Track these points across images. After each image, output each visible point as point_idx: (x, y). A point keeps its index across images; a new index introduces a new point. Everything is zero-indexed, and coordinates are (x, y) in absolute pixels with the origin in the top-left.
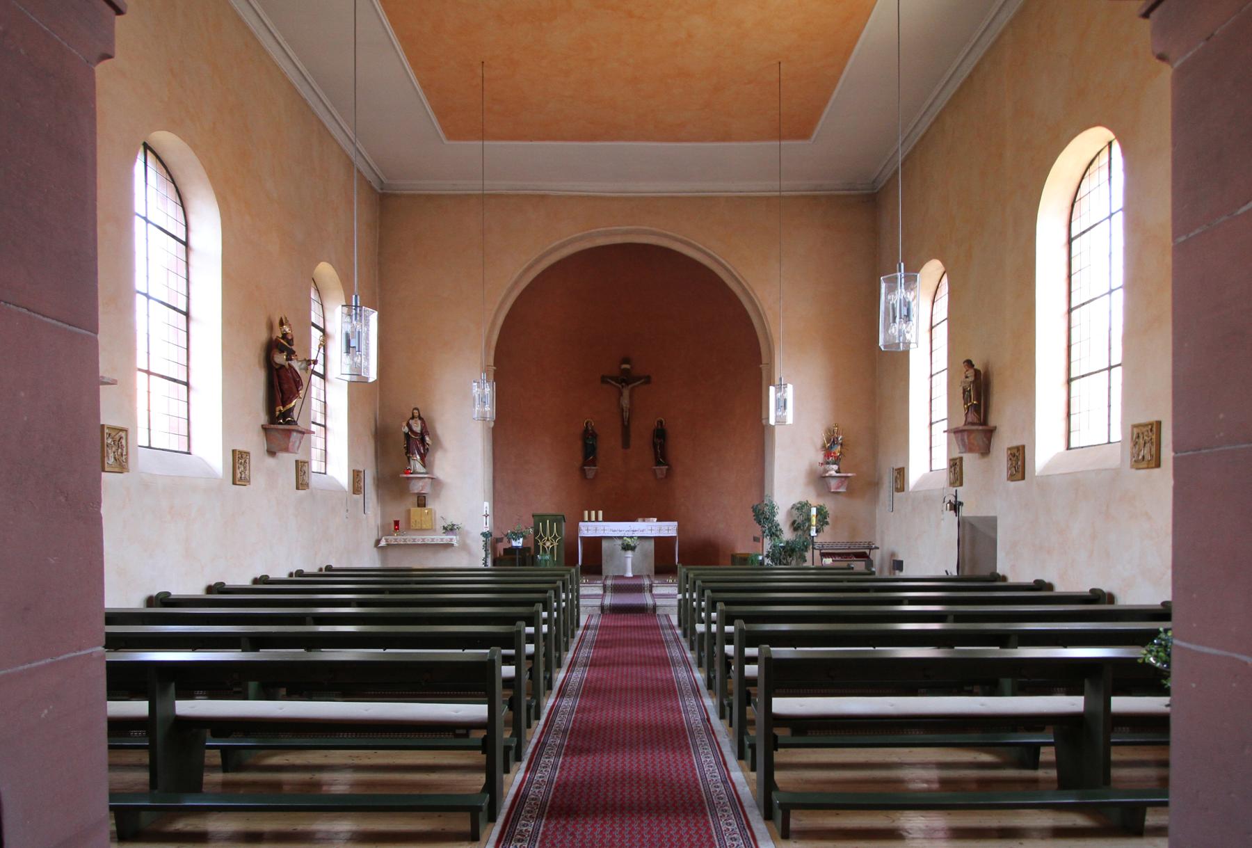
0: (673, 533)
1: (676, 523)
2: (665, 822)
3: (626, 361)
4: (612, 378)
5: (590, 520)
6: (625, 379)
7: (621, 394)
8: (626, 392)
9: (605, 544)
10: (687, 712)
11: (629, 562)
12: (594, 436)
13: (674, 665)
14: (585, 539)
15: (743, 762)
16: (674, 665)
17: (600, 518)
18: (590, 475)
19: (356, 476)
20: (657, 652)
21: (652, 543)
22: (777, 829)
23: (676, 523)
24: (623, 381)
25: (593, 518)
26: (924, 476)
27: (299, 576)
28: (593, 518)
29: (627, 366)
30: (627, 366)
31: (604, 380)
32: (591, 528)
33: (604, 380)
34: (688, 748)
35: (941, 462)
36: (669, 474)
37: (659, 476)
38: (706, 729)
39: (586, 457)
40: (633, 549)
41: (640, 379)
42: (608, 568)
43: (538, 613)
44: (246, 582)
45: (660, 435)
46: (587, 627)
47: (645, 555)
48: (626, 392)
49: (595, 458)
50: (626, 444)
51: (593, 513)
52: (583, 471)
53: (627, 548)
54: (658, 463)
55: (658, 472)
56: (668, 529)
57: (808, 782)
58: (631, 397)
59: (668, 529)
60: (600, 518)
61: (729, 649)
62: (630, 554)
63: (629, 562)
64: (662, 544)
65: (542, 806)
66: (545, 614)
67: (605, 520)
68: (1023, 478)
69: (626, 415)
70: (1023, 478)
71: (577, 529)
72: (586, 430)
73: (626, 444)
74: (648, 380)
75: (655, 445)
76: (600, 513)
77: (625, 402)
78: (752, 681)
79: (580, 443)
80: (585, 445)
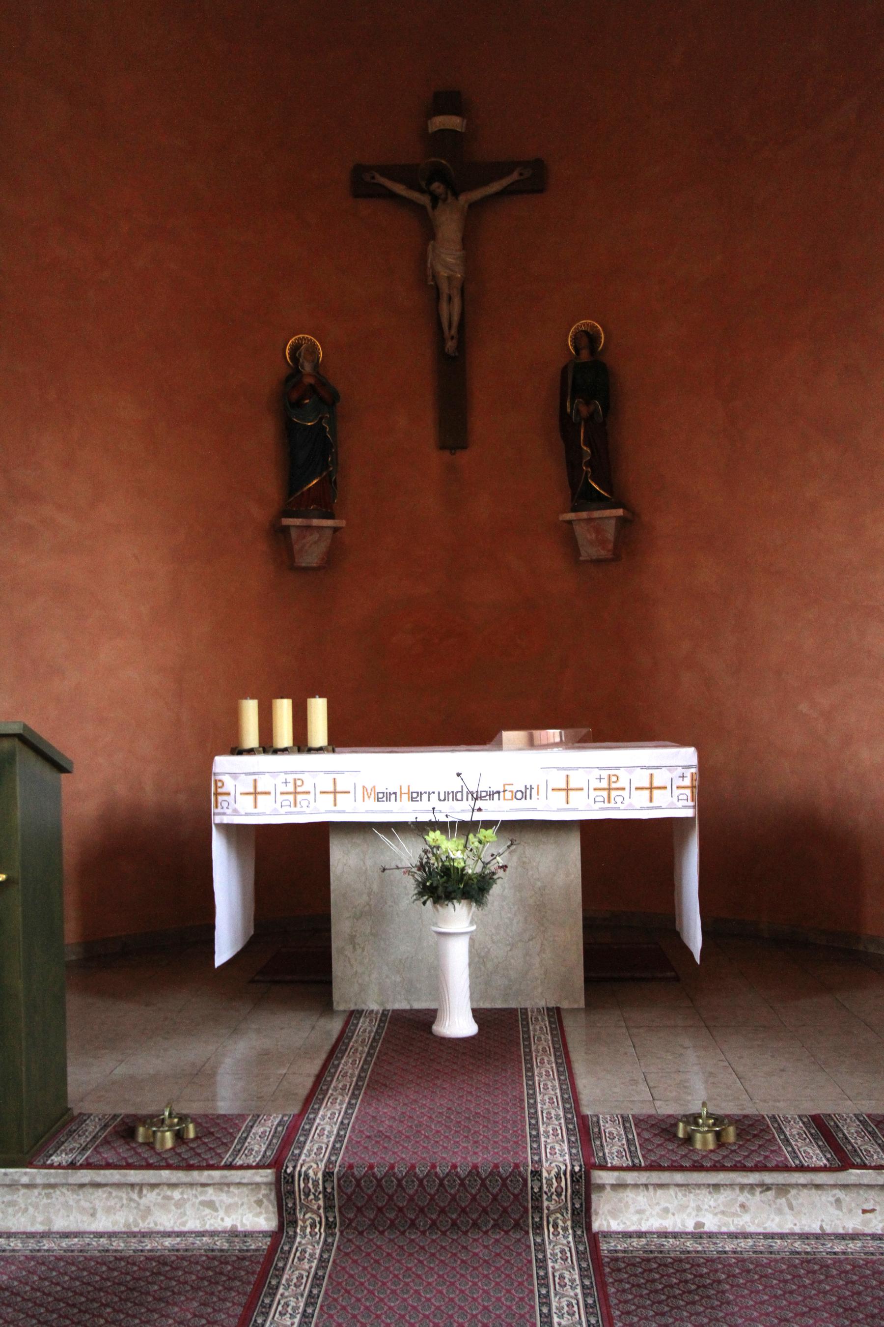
0: (676, 802)
1: (688, 755)
3: (448, 102)
4: (388, 171)
5: (267, 746)
6: (448, 169)
7: (430, 233)
8: (449, 224)
9: (343, 859)
11: (457, 961)
12: (324, 396)
14: (238, 834)
17: (319, 733)
18: (311, 553)
21: (571, 853)
23: (688, 755)
24: (438, 174)
25: (284, 735)
28: (284, 735)
29: (453, 122)
30: (453, 122)
31: (363, 185)
32: (273, 783)
33: (363, 185)
36: (629, 539)
37: (589, 551)
39: (293, 481)
40: (468, 888)
41: (499, 170)
42: (366, 981)
45: (589, 391)
47: (538, 911)
48: (449, 224)
49: (329, 486)
50: (453, 431)
51: (284, 709)
52: (279, 535)
53: (445, 885)
54: (584, 498)
55: (583, 534)
56: (649, 781)
57: (695, 938)
58: (469, 240)
59: (649, 781)
60: (319, 733)
62: (459, 918)
63: (457, 961)
64: (621, 855)
67: (342, 737)
69: (451, 311)
71: (202, 792)
72: (295, 372)
73: (453, 431)
74: (535, 179)
75: (567, 426)
76: (318, 708)
77: (447, 259)
79: (268, 431)
80: (289, 431)
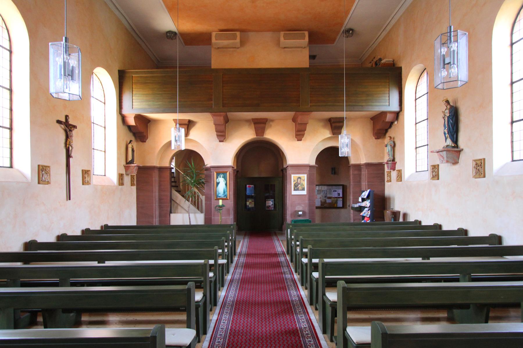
2: (282, 329)
10: (299, 322)
13: (283, 267)
15: (325, 335)
16: (283, 267)
19: (121, 177)
20: (274, 260)
22: (314, 309)
26: (507, 163)
27: (87, 232)
34: (286, 289)
35: (424, 165)
38: (300, 303)
43: (216, 251)
44: (52, 239)
46: (240, 255)
61: (305, 260)
65: (245, 254)
66: (226, 244)
68: (401, 181)
70: (401, 181)
78: (334, 304)
